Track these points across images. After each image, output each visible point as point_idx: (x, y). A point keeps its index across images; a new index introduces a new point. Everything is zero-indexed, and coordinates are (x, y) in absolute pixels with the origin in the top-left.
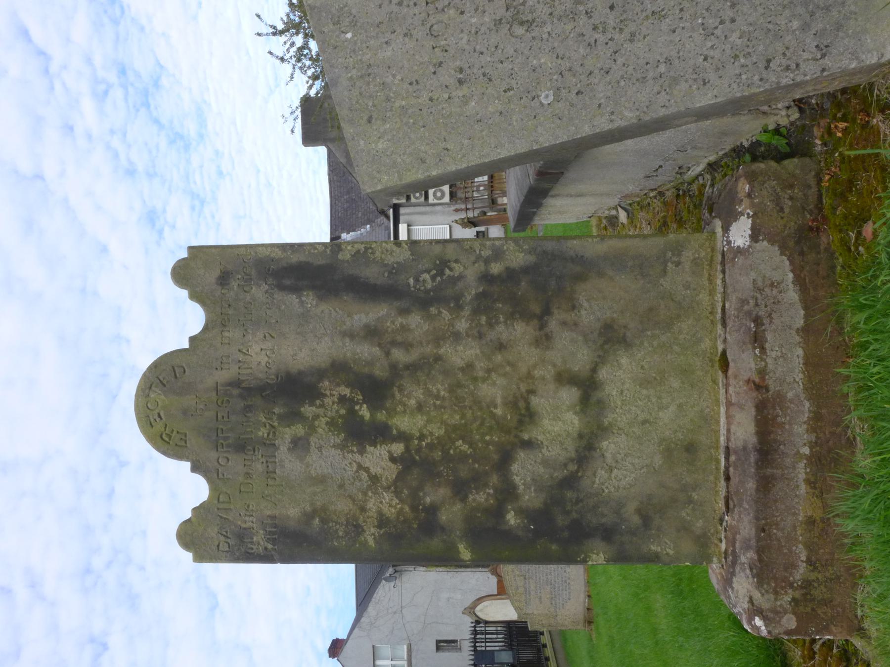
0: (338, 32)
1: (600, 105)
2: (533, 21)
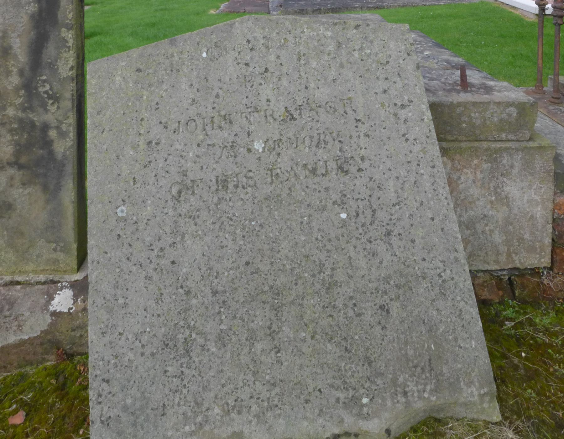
0: (209, 45)
1: (106, 253)
2: (179, 201)
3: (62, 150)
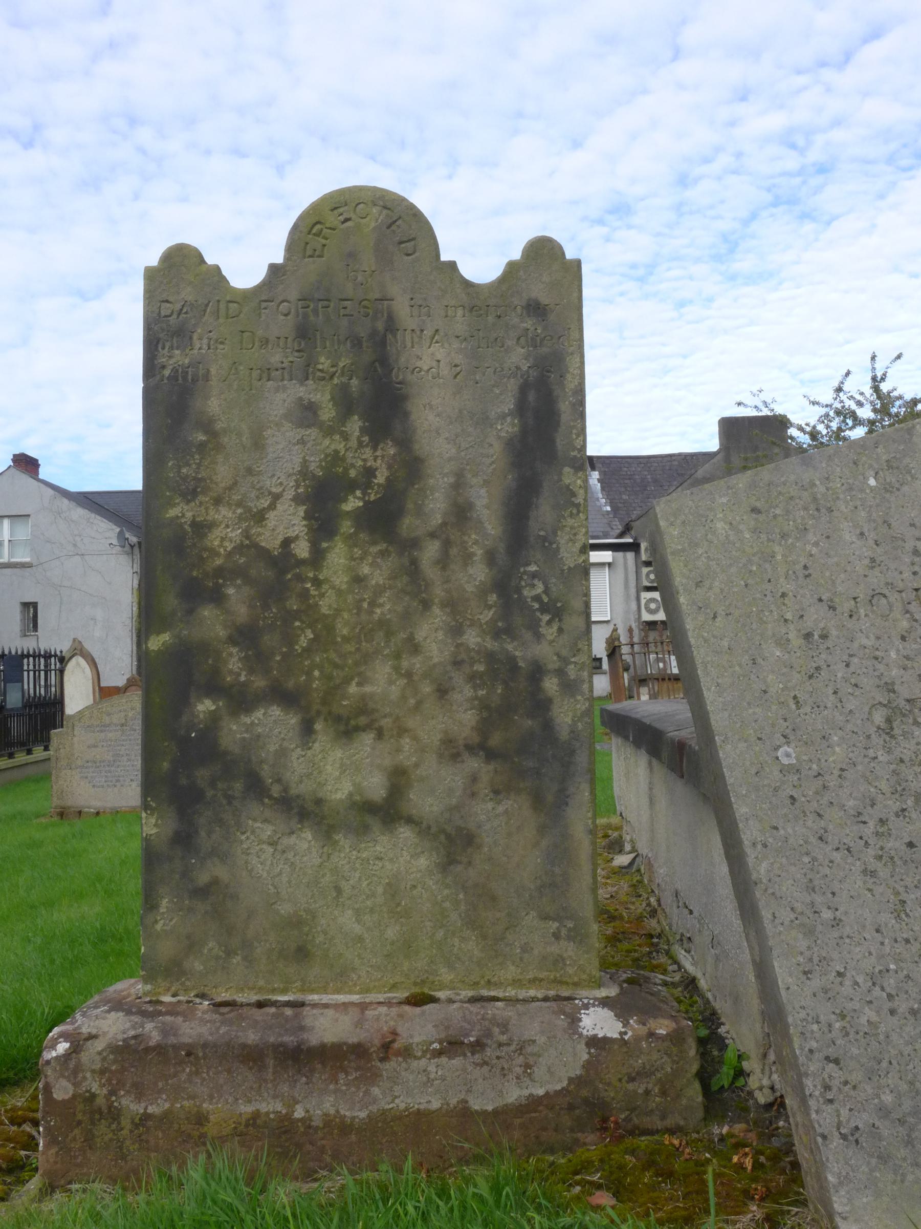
0: (876, 466)
1: (776, 828)
3: (568, 720)
